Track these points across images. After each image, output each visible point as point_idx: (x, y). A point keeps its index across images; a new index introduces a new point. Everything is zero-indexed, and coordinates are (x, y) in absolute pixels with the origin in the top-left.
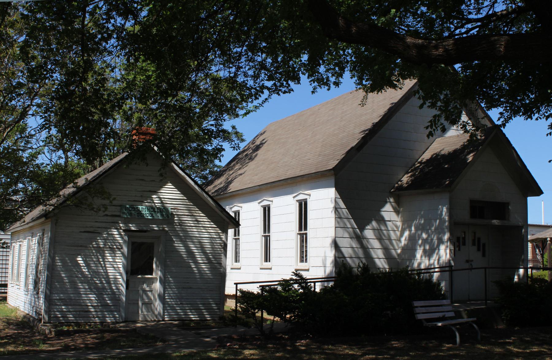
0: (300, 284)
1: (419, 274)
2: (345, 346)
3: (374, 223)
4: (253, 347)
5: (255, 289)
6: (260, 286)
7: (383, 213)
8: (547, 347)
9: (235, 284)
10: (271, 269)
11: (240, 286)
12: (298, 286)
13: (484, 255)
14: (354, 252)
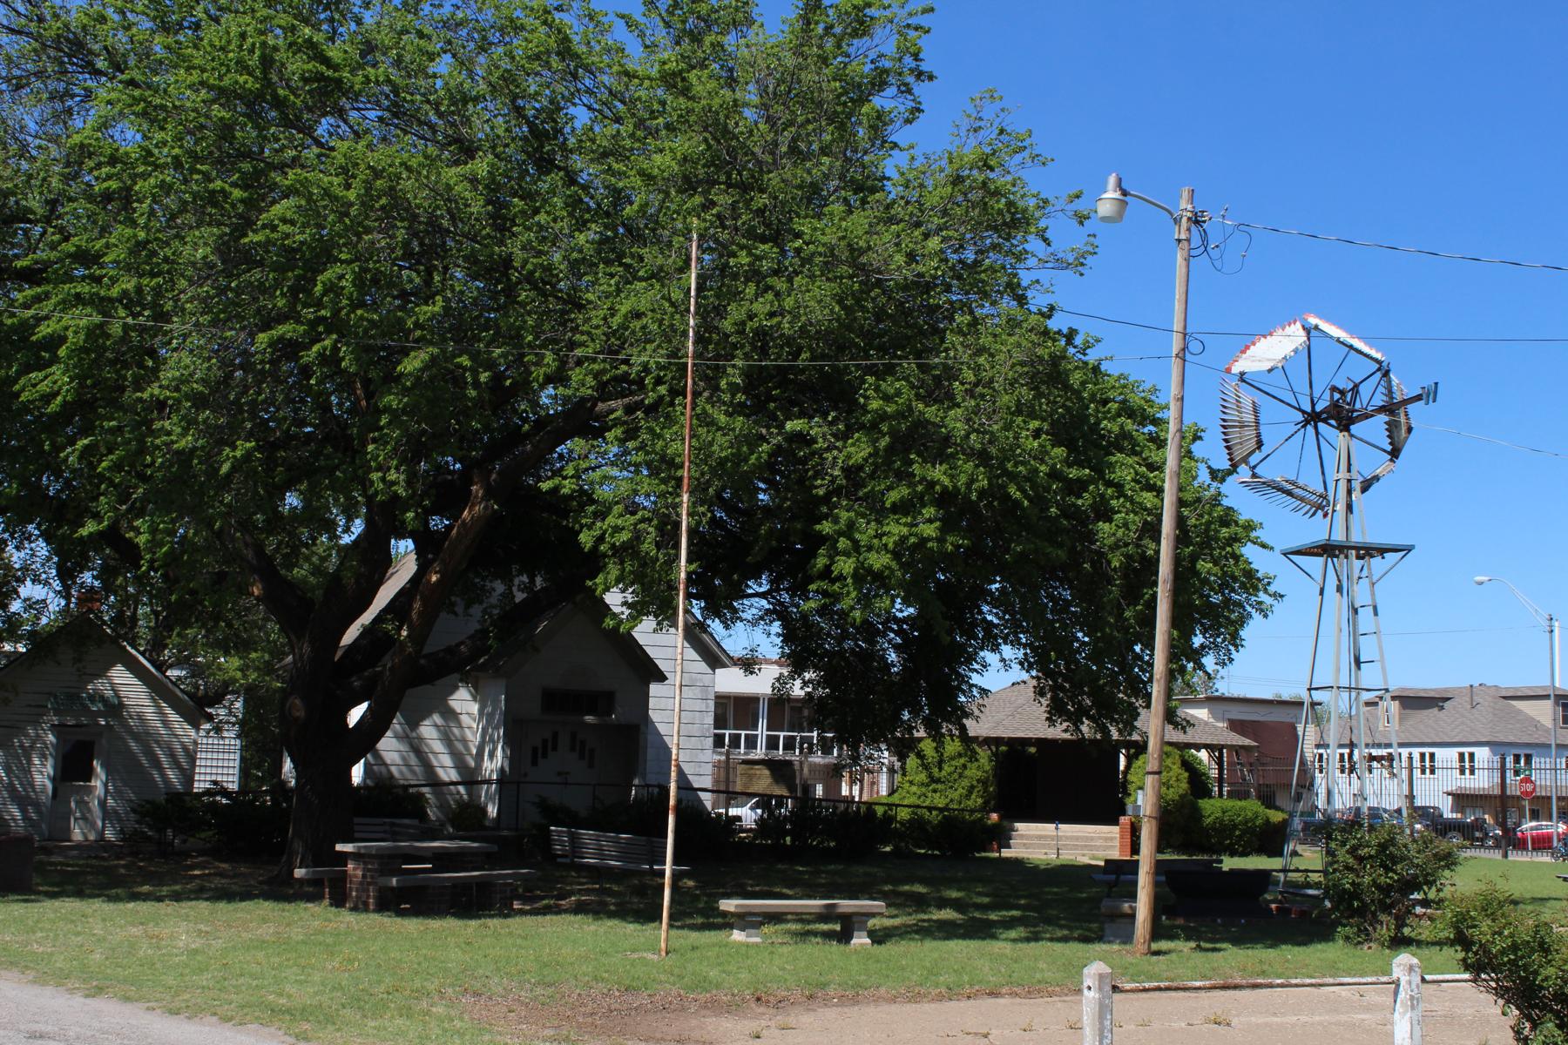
2: (225, 866)
3: (437, 718)
4: (910, 920)
7: (452, 703)
8: (985, 890)
14: (404, 759)
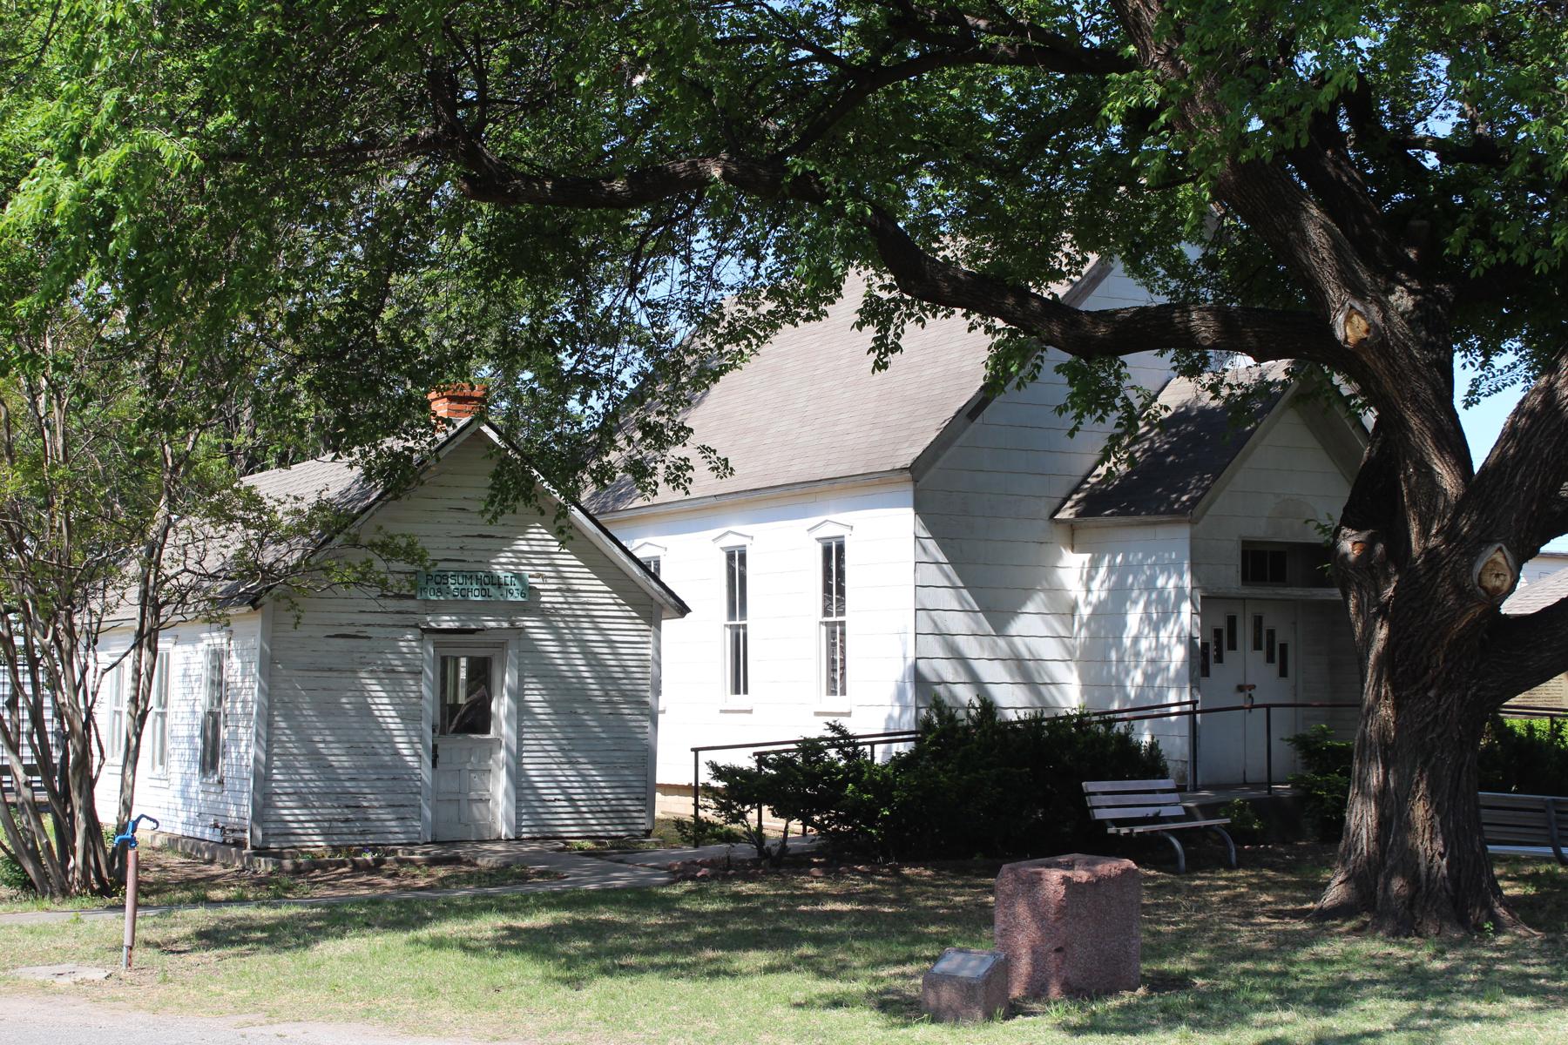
0: (840, 747)
1: (1109, 723)
5: (745, 760)
6: (755, 754)
9: (692, 750)
10: (750, 712)
11: (704, 757)
12: (838, 753)
13: (1283, 672)
